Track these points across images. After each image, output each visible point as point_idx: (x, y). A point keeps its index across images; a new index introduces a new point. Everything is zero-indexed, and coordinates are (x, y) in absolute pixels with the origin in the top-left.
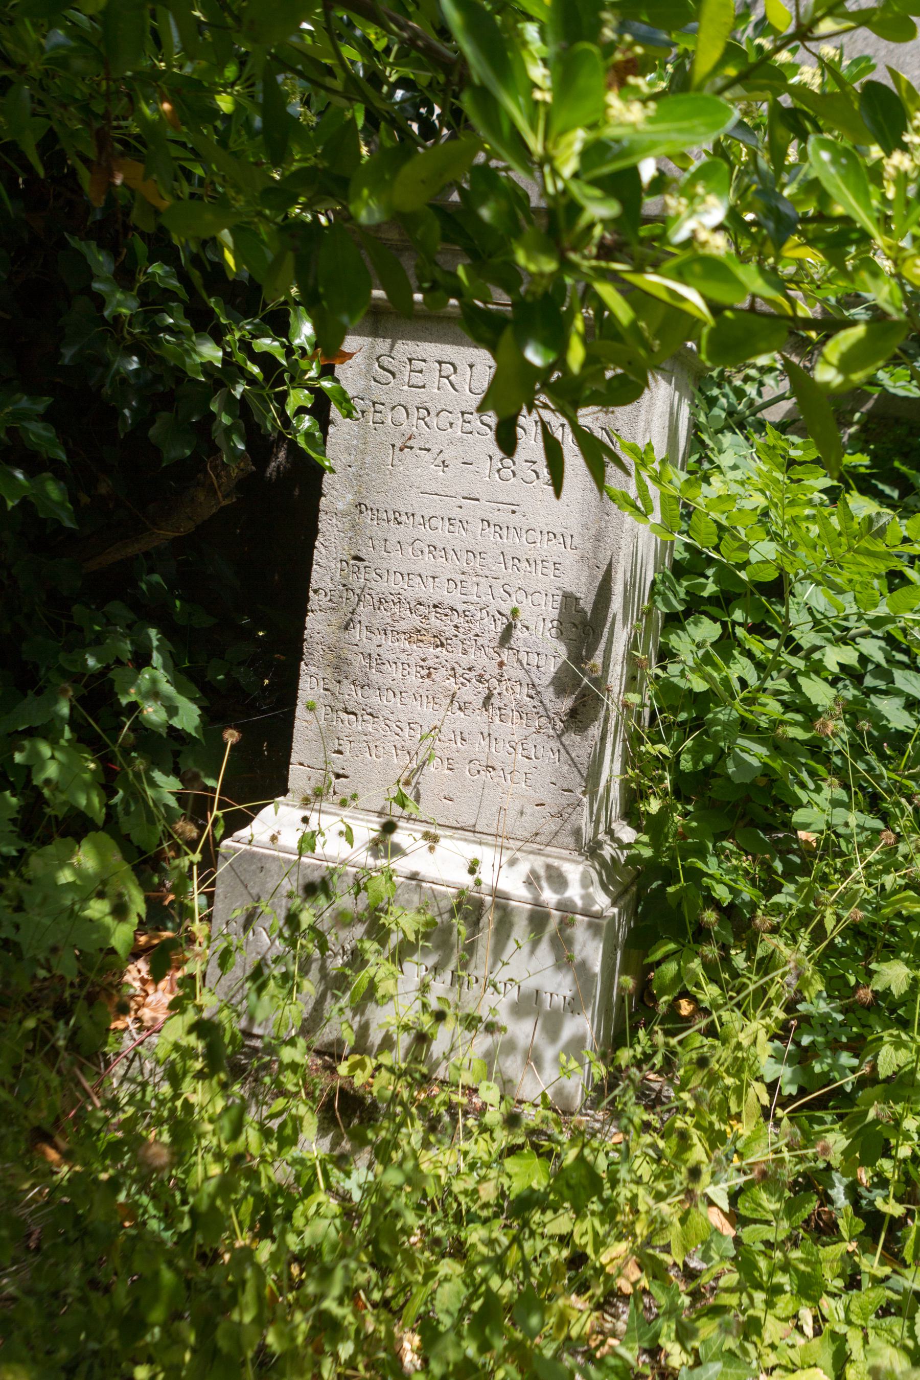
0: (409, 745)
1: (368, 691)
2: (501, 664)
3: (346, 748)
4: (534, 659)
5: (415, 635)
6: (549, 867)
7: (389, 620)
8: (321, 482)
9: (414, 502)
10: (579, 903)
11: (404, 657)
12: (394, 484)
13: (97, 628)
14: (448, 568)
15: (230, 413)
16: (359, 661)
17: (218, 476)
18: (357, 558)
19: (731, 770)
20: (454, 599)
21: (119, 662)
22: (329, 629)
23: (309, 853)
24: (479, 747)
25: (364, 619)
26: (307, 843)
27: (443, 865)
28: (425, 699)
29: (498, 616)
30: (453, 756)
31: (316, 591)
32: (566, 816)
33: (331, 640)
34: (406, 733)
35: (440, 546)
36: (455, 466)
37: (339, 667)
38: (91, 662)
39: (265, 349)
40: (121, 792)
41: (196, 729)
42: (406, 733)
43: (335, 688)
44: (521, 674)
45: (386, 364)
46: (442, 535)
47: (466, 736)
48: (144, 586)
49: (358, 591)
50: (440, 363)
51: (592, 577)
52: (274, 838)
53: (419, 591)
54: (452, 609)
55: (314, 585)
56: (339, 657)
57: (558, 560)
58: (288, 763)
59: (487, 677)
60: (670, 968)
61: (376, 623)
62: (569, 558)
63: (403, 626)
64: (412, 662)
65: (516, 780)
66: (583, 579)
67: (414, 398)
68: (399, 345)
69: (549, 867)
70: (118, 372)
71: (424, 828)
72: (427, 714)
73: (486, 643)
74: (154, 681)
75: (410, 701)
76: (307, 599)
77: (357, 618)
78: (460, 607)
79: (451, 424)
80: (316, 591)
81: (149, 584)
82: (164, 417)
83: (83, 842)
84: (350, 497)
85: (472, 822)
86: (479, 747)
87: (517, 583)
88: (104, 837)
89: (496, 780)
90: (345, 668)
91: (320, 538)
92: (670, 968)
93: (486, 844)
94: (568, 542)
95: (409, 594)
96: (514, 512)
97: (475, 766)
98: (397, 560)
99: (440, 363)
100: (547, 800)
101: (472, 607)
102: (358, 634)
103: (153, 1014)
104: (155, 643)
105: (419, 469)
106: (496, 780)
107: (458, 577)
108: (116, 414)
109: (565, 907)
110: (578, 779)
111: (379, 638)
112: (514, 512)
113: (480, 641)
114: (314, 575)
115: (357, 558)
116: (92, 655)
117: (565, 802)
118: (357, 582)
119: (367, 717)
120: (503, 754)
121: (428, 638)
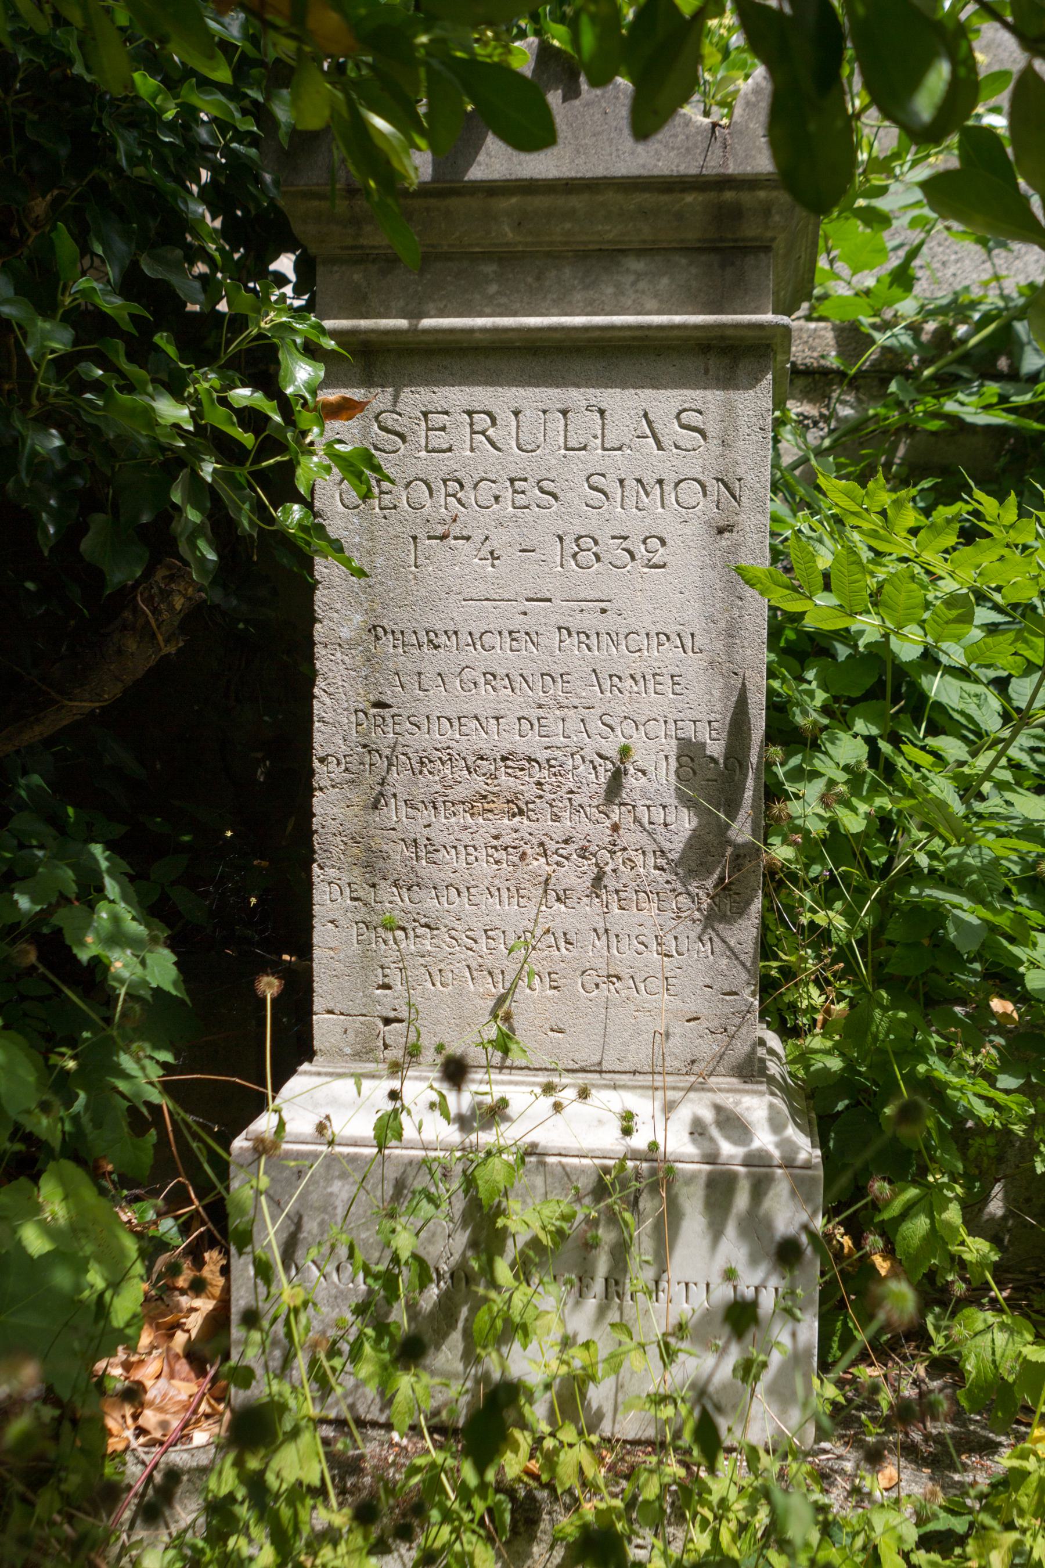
0: (488, 961)
1: (417, 894)
2: (615, 828)
3: (395, 979)
4: (659, 815)
5: (479, 804)
6: (718, 1109)
7: (438, 787)
8: (312, 602)
9: (458, 614)
10: (776, 1153)
11: (466, 837)
12: (423, 592)
13: (8, 855)
14: (515, 703)
15: (197, 507)
16: (399, 853)
17: (155, 611)
18: (379, 705)
19: (952, 934)
20: (532, 744)
21: (64, 899)
22: (349, 812)
23: (394, 1143)
24: (593, 952)
25: (400, 790)
26: (388, 1129)
27: (585, 1129)
28: (505, 894)
29: (598, 761)
30: (556, 968)
31: (322, 760)
32: (732, 1029)
33: (354, 826)
34: (483, 945)
35: (501, 672)
36: (510, 556)
37: (371, 864)
38: (24, 902)
39: (245, 403)
40: (82, 1096)
41: (175, 983)
42: (483, 945)
43: (368, 894)
44: (643, 838)
45: (390, 423)
46: (502, 657)
47: (572, 937)
48: (23, 793)
49: (387, 752)
50: (470, 413)
51: (727, 687)
52: (321, 1128)
53: (481, 741)
54: (530, 760)
55: (318, 751)
56: (369, 849)
57: (676, 671)
58: (310, 1013)
59: (593, 848)
60: (920, 1225)
61: (419, 794)
62: (693, 666)
63: (459, 792)
64: (480, 842)
65: (652, 988)
66: (717, 693)
67: (436, 466)
68: (407, 395)
69: (718, 1109)
70: (34, 453)
71: (542, 1078)
72: (512, 915)
73: (586, 801)
74: (116, 919)
75: (484, 899)
76: (311, 773)
77: (389, 790)
78: (542, 756)
79: (497, 498)
80: (322, 760)
81: (28, 788)
82: (98, 520)
83: (42, 1182)
84: (358, 618)
85: (596, 1059)
86: (593, 952)
87: (621, 711)
88: (69, 1167)
89: (624, 993)
90: (381, 864)
91: (320, 682)
92: (920, 1225)
93: (624, 1087)
94: (689, 644)
95: (463, 746)
96: (604, 611)
97: (590, 979)
98: (439, 700)
99: (470, 413)
100: (704, 1011)
101: (558, 753)
102: (392, 814)
103: (161, 1417)
104: (104, 865)
105: (459, 567)
106: (624, 993)
107: (534, 713)
108: (30, 523)
109: (756, 1161)
110: (744, 976)
111: (427, 815)
112: (604, 611)
113: (577, 799)
114: (317, 737)
115: (379, 705)
116: (22, 893)
117: (728, 1010)
118: (383, 739)
119: (421, 931)
120: (629, 955)
121: (500, 805)
